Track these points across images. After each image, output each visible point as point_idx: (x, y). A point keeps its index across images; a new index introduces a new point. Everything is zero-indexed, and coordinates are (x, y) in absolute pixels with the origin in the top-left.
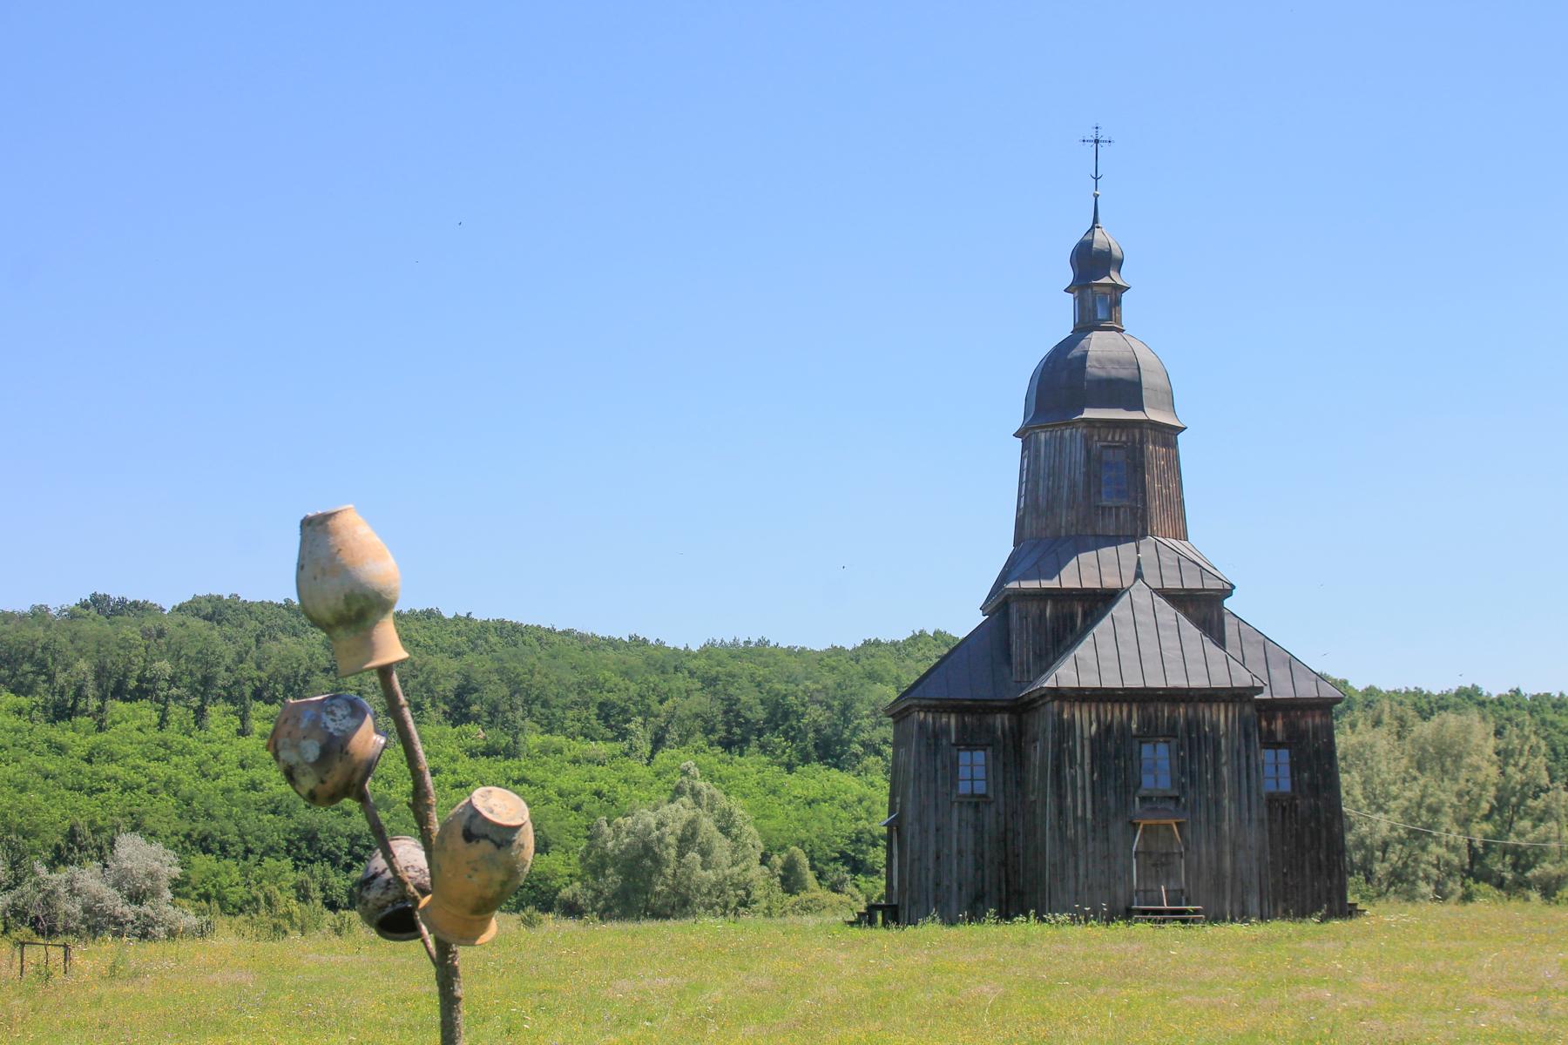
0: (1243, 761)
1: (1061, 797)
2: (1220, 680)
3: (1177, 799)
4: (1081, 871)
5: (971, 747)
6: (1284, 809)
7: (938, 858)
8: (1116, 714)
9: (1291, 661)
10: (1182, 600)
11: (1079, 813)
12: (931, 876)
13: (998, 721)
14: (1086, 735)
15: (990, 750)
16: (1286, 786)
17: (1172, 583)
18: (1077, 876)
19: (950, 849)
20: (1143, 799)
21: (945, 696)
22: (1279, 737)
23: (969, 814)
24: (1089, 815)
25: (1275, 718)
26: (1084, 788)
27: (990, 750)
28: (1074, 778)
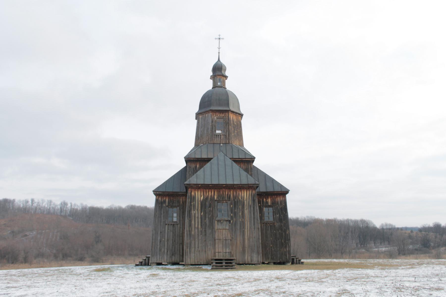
0: (252, 208)
1: (190, 221)
2: (244, 182)
3: (230, 221)
4: (196, 246)
5: (172, 207)
6: (271, 226)
7: (161, 242)
8: (210, 194)
9: (273, 180)
10: (238, 161)
11: (196, 226)
12: (158, 247)
13: (181, 199)
14: (199, 200)
15: (178, 208)
16: (271, 219)
17: (236, 156)
18: (195, 247)
19: (165, 239)
20: (218, 221)
21: (164, 191)
22: (269, 204)
23: (171, 228)
24: (200, 227)
25: (268, 198)
26: (198, 217)
27: (178, 208)
28: (195, 214)
